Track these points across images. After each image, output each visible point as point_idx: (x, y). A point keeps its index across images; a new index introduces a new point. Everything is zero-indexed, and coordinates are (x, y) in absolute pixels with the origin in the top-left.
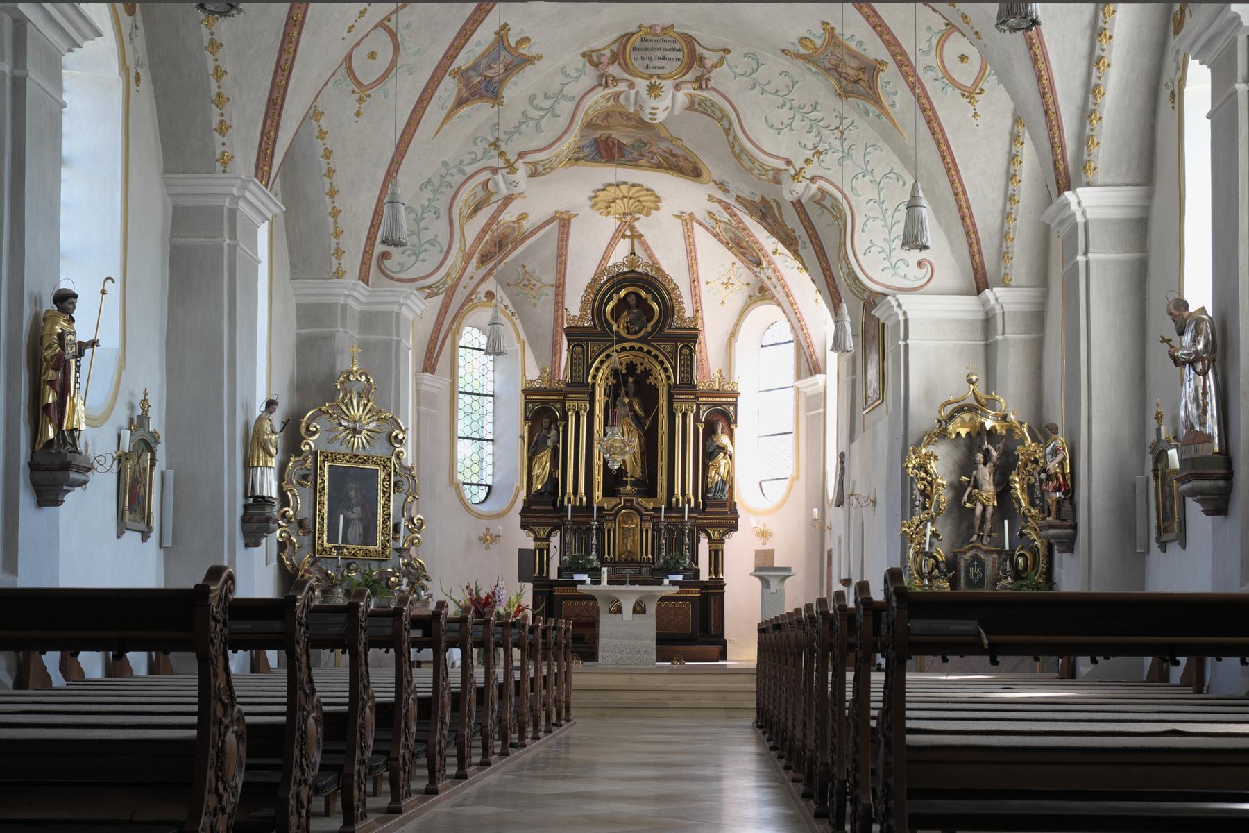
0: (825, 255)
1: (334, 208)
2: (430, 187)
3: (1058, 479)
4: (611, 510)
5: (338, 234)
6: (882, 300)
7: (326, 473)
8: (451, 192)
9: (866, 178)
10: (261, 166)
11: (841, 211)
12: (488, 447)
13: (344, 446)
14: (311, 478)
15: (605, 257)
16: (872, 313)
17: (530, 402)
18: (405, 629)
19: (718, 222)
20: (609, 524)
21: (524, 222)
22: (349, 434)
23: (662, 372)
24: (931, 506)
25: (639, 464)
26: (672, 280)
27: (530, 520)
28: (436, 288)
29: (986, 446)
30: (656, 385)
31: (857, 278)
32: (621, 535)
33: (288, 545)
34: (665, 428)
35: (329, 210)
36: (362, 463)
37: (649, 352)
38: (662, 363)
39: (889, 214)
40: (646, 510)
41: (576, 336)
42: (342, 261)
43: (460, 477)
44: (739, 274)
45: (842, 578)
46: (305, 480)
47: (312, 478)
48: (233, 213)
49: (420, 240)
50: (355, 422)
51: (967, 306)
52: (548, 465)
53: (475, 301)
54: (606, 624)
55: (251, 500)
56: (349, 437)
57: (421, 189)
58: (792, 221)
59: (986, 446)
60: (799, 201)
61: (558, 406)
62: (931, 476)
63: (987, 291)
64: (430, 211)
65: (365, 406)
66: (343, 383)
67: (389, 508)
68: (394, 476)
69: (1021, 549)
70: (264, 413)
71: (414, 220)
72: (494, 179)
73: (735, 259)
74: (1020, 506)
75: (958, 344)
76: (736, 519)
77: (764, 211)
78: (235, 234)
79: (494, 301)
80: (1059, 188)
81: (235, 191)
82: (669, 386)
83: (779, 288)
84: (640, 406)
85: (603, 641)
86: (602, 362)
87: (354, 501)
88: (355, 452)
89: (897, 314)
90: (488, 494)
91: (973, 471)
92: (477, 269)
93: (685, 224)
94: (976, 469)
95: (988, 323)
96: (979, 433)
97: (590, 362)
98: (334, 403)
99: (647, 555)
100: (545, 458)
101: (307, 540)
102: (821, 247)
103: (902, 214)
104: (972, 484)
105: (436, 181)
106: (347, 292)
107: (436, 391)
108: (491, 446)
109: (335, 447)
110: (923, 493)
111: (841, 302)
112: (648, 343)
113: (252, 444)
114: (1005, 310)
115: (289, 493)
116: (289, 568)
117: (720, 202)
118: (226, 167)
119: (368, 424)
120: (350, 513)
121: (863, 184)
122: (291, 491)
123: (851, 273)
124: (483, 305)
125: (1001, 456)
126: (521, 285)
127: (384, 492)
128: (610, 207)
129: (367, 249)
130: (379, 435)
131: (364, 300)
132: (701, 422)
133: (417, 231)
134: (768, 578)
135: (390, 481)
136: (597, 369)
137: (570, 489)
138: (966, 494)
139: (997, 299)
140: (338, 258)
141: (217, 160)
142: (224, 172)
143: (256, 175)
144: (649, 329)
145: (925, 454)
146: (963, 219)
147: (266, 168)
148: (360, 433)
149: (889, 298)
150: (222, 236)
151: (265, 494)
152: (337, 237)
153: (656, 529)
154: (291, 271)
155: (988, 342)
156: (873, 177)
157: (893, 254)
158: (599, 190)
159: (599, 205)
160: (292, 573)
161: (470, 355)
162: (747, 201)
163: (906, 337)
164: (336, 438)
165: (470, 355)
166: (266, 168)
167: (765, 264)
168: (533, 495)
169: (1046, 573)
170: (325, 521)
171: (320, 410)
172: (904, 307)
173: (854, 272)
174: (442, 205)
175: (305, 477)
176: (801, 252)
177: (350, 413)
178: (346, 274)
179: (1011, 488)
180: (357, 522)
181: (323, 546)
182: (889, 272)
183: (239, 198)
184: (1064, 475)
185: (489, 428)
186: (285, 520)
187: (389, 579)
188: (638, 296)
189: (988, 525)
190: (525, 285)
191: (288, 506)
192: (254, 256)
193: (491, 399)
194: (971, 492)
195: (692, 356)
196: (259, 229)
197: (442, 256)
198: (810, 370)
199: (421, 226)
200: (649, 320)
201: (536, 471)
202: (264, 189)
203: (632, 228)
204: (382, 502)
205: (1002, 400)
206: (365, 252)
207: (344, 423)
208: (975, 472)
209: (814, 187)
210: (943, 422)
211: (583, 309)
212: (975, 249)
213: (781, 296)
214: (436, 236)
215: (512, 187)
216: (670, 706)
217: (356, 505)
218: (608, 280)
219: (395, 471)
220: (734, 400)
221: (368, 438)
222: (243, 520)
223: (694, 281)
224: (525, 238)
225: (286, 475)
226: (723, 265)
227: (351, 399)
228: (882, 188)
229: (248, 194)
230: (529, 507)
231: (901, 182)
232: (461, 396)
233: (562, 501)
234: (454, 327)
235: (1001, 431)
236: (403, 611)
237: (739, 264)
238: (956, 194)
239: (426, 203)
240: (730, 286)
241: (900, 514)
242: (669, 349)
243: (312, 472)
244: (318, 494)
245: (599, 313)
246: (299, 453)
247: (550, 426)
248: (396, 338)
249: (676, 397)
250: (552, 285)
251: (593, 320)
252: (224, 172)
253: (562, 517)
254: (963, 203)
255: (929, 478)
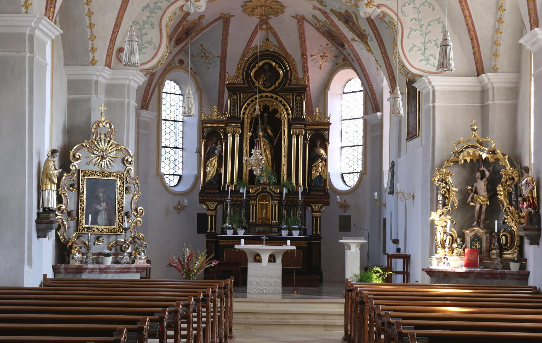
0: (384, 46)
1: (91, 23)
2: (148, 9)
3: (529, 201)
4: (254, 193)
5: (93, 38)
6: (419, 78)
7: (85, 183)
8: (161, 12)
9: (410, 6)
10: (48, 8)
11: (397, 32)
12: (180, 152)
13: (96, 166)
14: (76, 186)
15: (251, 40)
16: (413, 85)
17: (205, 128)
18: (145, 339)
19: (318, 21)
20: (253, 202)
21: (202, 20)
22: (99, 159)
23: (284, 111)
24: (449, 203)
25: (271, 165)
26: (291, 56)
27: (205, 198)
28: (152, 69)
29: (482, 168)
30: (280, 118)
31: (404, 66)
32: (260, 208)
33: (62, 227)
34: (286, 144)
35: (88, 24)
36: (107, 176)
37: (277, 99)
38: (284, 105)
39: (424, 27)
40: (275, 193)
41: (233, 89)
42: (95, 55)
43: (163, 171)
44: (330, 51)
45: (393, 238)
46: (72, 188)
47: (76, 186)
48: (31, 37)
49: (142, 41)
50: (103, 152)
51: (469, 82)
52: (216, 165)
53: (173, 65)
54: (252, 268)
55: (41, 210)
56: (99, 161)
57: (143, 10)
58: (365, 27)
59: (482, 168)
60: (370, 17)
61: (222, 130)
62: (449, 186)
63: (483, 75)
64: (148, 24)
65: (109, 142)
66: (96, 128)
67: (123, 203)
68: (126, 183)
69: (504, 231)
70: (50, 158)
71: (139, 29)
72: (187, 5)
73: (328, 42)
74: (503, 206)
75: (465, 106)
76: (329, 199)
77: (347, 18)
78: (33, 50)
79: (184, 65)
80: (531, 25)
81: (33, 24)
82: (289, 119)
83: (355, 60)
84: (271, 130)
85: (250, 279)
86: (248, 105)
87: (102, 199)
88: (103, 170)
89: (428, 87)
90: (180, 180)
91: (474, 183)
92: (174, 47)
93: (298, 21)
94: (476, 182)
95: (483, 93)
96: (478, 160)
97: (241, 104)
98: (90, 141)
99: (275, 220)
100: (214, 161)
101: (73, 223)
102: (382, 41)
103: (437, 52)
104: (474, 190)
105: (152, 6)
106: (98, 73)
107: (149, 120)
108: (181, 152)
109: (91, 167)
110: (443, 196)
111: (396, 86)
112: (276, 93)
113: (43, 176)
114: (494, 86)
115: (62, 195)
116: (62, 240)
117: (320, 10)
118: (27, 10)
119: (110, 153)
120: (99, 206)
121: (408, 9)
122: (64, 194)
123: (401, 62)
124: (177, 68)
125: (491, 175)
126: (200, 56)
127: (120, 194)
128: (254, 11)
129: (110, 47)
130: (117, 159)
131: (108, 77)
132: (308, 141)
133: (140, 36)
134: (349, 244)
135: (123, 186)
136: (246, 109)
137: (228, 180)
138: (470, 197)
139: (489, 80)
140: (93, 53)
141: (22, 6)
142: (26, 13)
143: (46, 15)
144: (277, 85)
145: (446, 173)
146: (469, 31)
147: (52, 10)
148: (105, 158)
149: (424, 78)
150: (25, 51)
151: (50, 206)
152: (92, 40)
153: (280, 205)
154: (64, 60)
155: (484, 104)
156: (415, 4)
157: (426, 51)
158: (247, 2)
159: (248, 10)
160: (64, 243)
161: (169, 97)
162: (337, 12)
163: (434, 102)
164: (91, 161)
165: (169, 97)
166: (52, 10)
167: (347, 46)
168: (207, 183)
169: (519, 247)
170: (85, 212)
171: (82, 145)
172: (433, 84)
173: (402, 62)
174: (155, 20)
175: (72, 186)
176: (369, 43)
177: (100, 146)
178: (98, 63)
179: (498, 194)
180: (104, 212)
181: (83, 227)
182: (424, 62)
183: (35, 28)
184: (532, 197)
185: (181, 141)
186: (60, 212)
187: (122, 246)
188: (270, 65)
189: (483, 217)
190: (202, 56)
191: (62, 203)
192: (45, 62)
193: (181, 123)
194: (473, 196)
195: (302, 101)
196: (47, 45)
197: (155, 51)
198: (373, 109)
199: (143, 33)
200: (277, 79)
201: (209, 169)
202: (50, 21)
203: (267, 23)
204: (119, 200)
205: (492, 142)
206: (109, 48)
207: (95, 152)
208: (475, 184)
209: (379, 11)
210: (456, 154)
211: (237, 72)
212: (476, 48)
213: (357, 66)
214: (152, 39)
215: (197, 9)
216: (291, 323)
217: (103, 202)
218: (252, 56)
219: (126, 180)
220: (327, 127)
221: (110, 161)
222: (37, 222)
223: (304, 55)
224: (204, 29)
225: (61, 185)
226: (321, 46)
227: (100, 138)
228: (420, 12)
229: (41, 26)
230: (204, 190)
231: (432, 8)
232: (163, 122)
233: (224, 187)
234: (160, 82)
235: (491, 160)
236: (144, 328)
237: (330, 45)
238: (465, 17)
239: (146, 19)
240: (325, 58)
241: (430, 207)
242: (289, 97)
243: (76, 182)
244: (80, 196)
245: (247, 76)
246: (69, 171)
247: (217, 142)
248: (127, 100)
249: (293, 126)
250: (219, 57)
251: (243, 79)
252: (26, 13)
253: (224, 197)
254: (470, 22)
255: (448, 187)
